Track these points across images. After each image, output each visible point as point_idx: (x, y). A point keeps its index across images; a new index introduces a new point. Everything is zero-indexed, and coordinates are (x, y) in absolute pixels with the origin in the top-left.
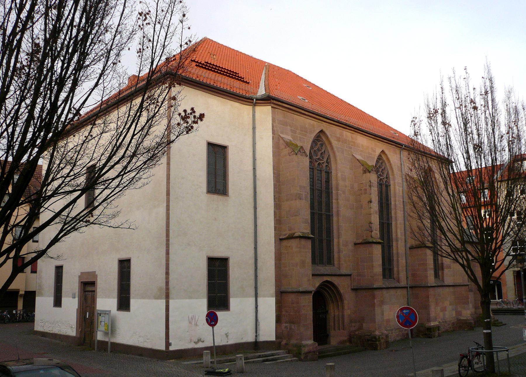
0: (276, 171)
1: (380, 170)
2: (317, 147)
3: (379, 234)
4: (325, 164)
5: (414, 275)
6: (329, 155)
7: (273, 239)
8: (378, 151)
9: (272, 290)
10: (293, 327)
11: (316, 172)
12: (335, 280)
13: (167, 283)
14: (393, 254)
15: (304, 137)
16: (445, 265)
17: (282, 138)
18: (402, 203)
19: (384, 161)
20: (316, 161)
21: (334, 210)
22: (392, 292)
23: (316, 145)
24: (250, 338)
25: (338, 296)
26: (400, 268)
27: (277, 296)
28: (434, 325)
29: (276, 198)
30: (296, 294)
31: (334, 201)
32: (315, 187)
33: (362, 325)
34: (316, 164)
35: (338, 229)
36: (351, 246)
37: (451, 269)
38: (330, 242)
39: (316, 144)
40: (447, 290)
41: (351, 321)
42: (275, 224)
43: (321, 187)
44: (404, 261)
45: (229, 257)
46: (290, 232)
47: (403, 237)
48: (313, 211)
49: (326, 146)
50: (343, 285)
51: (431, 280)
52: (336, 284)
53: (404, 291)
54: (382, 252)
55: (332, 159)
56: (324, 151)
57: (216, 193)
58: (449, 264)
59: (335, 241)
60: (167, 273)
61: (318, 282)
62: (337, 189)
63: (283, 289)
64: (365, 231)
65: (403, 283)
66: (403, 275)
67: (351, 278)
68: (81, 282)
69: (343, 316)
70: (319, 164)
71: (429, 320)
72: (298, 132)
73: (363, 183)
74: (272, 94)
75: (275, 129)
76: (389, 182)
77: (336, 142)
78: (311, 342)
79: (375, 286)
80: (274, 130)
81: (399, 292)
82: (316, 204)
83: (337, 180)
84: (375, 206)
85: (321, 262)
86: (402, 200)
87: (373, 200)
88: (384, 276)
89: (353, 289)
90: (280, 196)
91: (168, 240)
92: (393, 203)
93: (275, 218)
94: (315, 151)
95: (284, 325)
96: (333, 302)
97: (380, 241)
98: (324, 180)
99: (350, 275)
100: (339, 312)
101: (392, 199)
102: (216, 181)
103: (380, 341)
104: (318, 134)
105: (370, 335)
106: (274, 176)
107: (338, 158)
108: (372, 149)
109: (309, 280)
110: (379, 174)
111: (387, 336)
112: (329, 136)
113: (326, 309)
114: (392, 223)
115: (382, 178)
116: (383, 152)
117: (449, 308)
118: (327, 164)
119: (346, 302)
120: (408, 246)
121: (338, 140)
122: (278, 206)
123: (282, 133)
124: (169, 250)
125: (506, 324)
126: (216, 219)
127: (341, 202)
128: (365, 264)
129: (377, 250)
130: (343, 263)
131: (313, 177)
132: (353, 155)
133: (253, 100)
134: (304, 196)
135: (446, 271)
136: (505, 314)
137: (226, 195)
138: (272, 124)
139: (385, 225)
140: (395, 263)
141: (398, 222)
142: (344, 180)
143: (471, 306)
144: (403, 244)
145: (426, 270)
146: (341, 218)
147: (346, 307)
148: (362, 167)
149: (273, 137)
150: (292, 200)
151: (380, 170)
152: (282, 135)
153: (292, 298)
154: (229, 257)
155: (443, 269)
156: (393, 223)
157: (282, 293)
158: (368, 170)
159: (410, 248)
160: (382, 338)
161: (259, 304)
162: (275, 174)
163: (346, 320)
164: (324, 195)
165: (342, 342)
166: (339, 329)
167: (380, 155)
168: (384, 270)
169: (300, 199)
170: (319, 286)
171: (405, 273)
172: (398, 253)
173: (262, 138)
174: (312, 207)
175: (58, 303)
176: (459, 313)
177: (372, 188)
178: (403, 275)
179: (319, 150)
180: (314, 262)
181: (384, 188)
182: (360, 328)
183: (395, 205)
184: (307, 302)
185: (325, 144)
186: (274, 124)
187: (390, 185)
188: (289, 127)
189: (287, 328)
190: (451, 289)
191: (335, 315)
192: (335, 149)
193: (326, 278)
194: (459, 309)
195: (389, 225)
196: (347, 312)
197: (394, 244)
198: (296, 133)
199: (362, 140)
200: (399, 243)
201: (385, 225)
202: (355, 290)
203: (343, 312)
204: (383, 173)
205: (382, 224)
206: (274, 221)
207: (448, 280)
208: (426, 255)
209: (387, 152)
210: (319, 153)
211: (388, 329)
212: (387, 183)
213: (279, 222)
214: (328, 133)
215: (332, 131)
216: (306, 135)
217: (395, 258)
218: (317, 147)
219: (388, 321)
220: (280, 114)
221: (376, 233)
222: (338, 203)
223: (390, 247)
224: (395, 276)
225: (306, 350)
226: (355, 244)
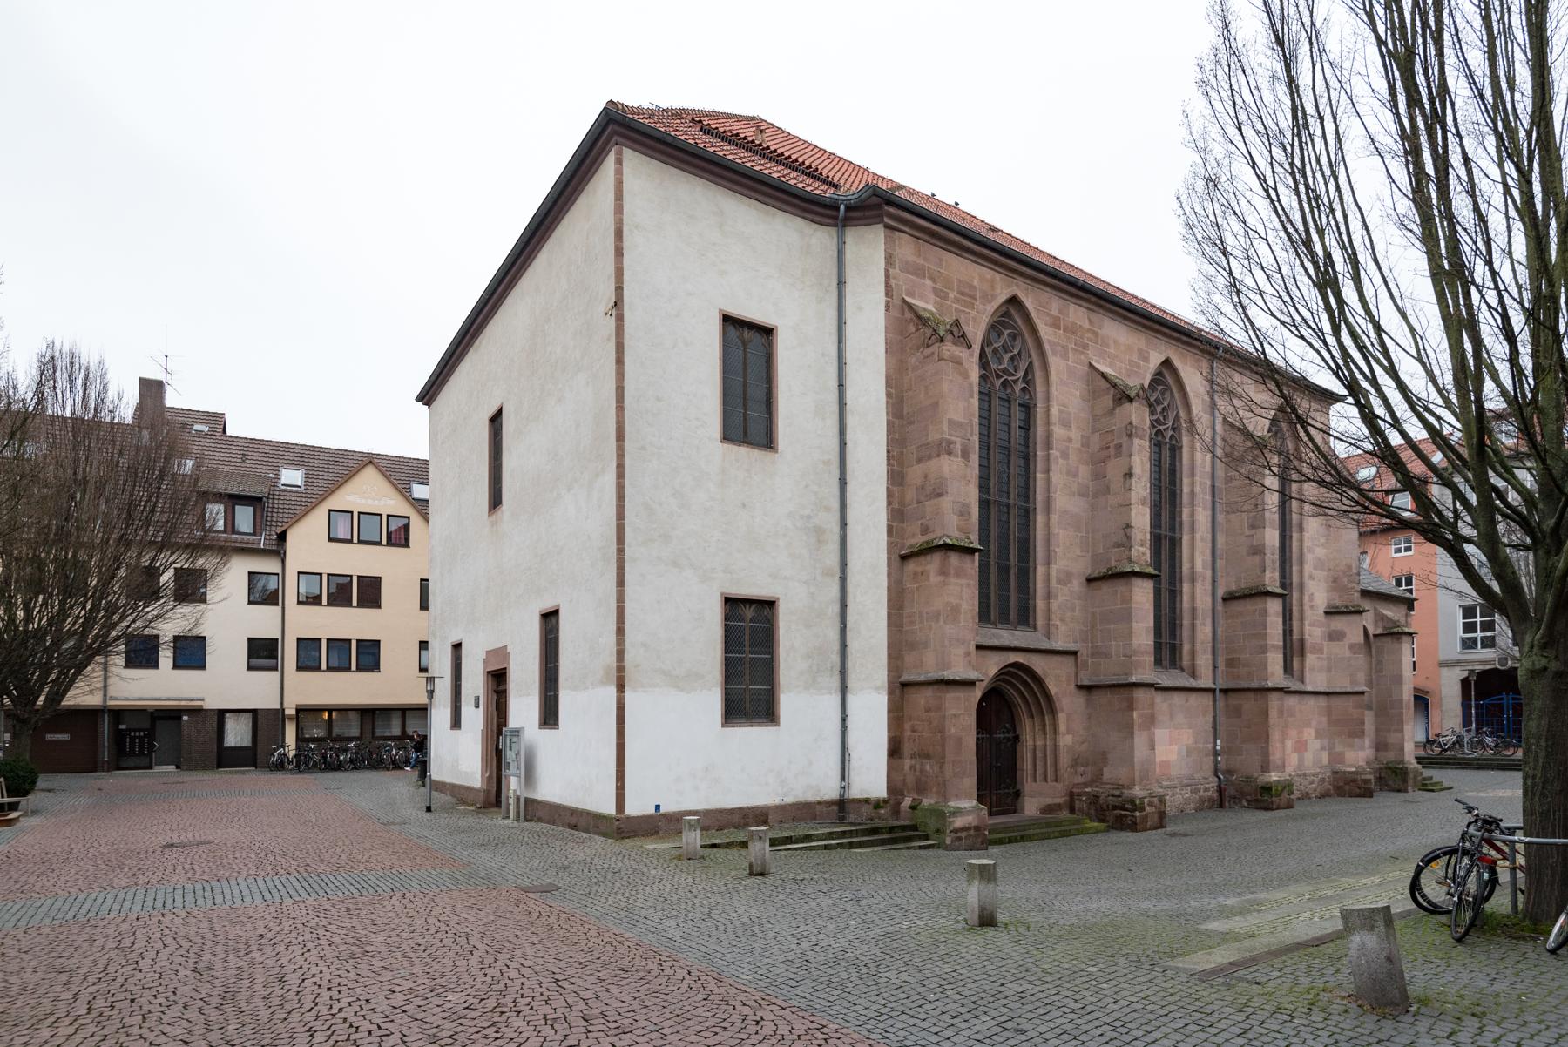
0: (893, 391)
1: (1159, 409)
2: (1002, 340)
3: (1149, 555)
4: (1021, 385)
5: (1231, 663)
6: (1031, 364)
7: (884, 556)
8: (1156, 359)
9: (881, 676)
10: (928, 767)
11: (996, 402)
12: (1037, 663)
13: (620, 654)
14: (1181, 611)
15: (967, 310)
16: (1308, 646)
17: (910, 306)
18: (1208, 490)
19: (1168, 388)
20: (998, 377)
21: (1040, 496)
22: (1178, 698)
23: (999, 336)
24: (830, 791)
25: (1044, 704)
26: (1198, 645)
27: (891, 693)
28: (1278, 781)
29: (893, 456)
30: (936, 687)
31: (1039, 475)
32: (992, 439)
33: (1101, 770)
34: (998, 383)
35: (1048, 541)
36: (1077, 585)
37: (1322, 653)
38: (1026, 575)
39: (1000, 335)
40: (1311, 702)
41: (1075, 763)
42: (888, 520)
43: (1009, 442)
44: (1208, 629)
45: (778, 599)
46: (925, 538)
47: (1209, 573)
48: (987, 496)
49: (1024, 342)
50: (1057, 677)
51: (1275, 673)
52: (1039, 671)
53: (1207, 700)
54: (1155, 597)
55: (1038, 373)
56: (1019, 353)
57: (745, 442)
58: (1319, 642)
59: (1040, 570)
60: (621, 631)
61: (992, 666)
62: (1048, 445)
63: (905, 677)
64: (1114, 547)
65: (1205, 681)
66: (1204, 661)
67: (1076, 659)
68: (488, 672)
69: (1055, 747)
70: (1005, 384)
71: (1265, 768)
72: (951, 295)
73: (1112, 431)
74: (821, 238)
75: (893, 282)
76: (1179, 440)
77: (1051, 330)
78: (969, 803)
79: (1134, 679)
80: (891, 287)
81: (1194, 699)
82: (994, 481)
83: (1048, 423)
84: (1141, 487)
85: (1005, 619)
86: (1209, 483)
87: (1137, 470)
88: (1158, 662)
89: (1080, 687)
90: (902, 453)
91: (621, 551)
92: (1186, 490)
93: (889, 503)
94: (995, 351)
95: (908, 763)
96: (1032, 716)
97: (1152, 571)
98: (1016, 424)
99: (1074, 653)
100: (1046, 738)
101: (1186, 481)
102: (745, 415)
103: (1142, 809)
104: (1004, 309)
105: (1119, 796)
106: (887, 402)
107: (1053, 371)
108: (1140, 351)
109: (968, 654)
110: (1155, 417)
111: (1162, 800)
112: (1033, 314)
113: (1015, 732)
114: (1181, 539)
115: (1161, 427)
116: (1167, 363)
117: (1314, 744)
118: (1024, 385)
119: (1062, 717)
120: (1220, 593)
121: (1055, 324)
122: (896, 477)
123: (911, 295)
124: (623, 575)
125: (1451, 788)
126: (744, 506)
127: (1057, 478)
128: (1112, 626)
129: (1143, 594)
130: (1058, 623)
131: (990, 416)
132: (1091, 365)
133: (838, 209)
134: (959, 446)
135: (1311, 659)
136: (1441, 768)
137: (771, 448)
138: (887, 271)
139: (1165, 545)
140: (1186, 633)
141: (1198, 536)
142: (1066, 424)
143: (1367, 742)
144: (1209, 587)
145: (1264, 649)
146: (1054, 518)
147: (1062, 727)
148: (1112, 391)
149: (887, 303)
150: (930, 458)
151: (1159, 409)
152: (909, 300)
153: (922, 698)
154: (778, 599)
155: (1302, 654)
156: (1186, 539)
157: (905, 685)
158: (1128, 396)
159: (1224, 600)
160: (1151, 804)
161: (849, 712)
162: (891, 398)
163: (1064, 760)
164: (1016, 461)
165: (1049, 809)
166: (1046, 780)
167: (1159, 373)
168: (1158, 646)
169: (950, 453)
170: (997, 675)
171: (1210, 656)
172: (1194, 610)
173: (860, 309)
174: (984, 486)
175: (456, 723)
176: (1336, 757)
177: (1136, 441)
178: (1204, 661)
179: (1006, 349)
180: (984, 616)
181: (1166, 454)
182: (1097, 779)
183: (1192, 493)
184: (961, 713)
185: (1021, 334)
186: (891, 271)
187: (1181, 447)
188: (928, 282)
189: (915, 770)
190: (1322, 701)
191: (1035, 746)
192: (1047, 347)
193: (1013, 658)
194: (1339, 748)
195: (1175, 544)
196: (1065, 740)
197: (1186, 587)
198: (946, 297)
199: (1116, 332)
200: (1199, 585)
201: (1165, 545)
202: (1087, 689)
203: (1055, 739)
204: (1165, 417)
205: (1156, 540)
206: (888, 514)
207: (1316, 679)
208: (1264, 613)
209: (1177, 363)
210: (1006, 357)
211: (1165, 783)
212: (1174, 442)
213: (898, 514)
214: (1029, 303)
215: (1041, 305)
216: (972, 306)
217: (1186, 622)
218: (1002, 340)
219: (1166, 764)
220: (907, 247)
221: (1141, 553)
222: (1048, 481)
223: (1174, 594)
224: (1186, 662)
225: (959, 822)
226: (1090, 580)
